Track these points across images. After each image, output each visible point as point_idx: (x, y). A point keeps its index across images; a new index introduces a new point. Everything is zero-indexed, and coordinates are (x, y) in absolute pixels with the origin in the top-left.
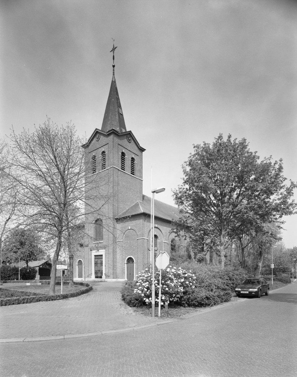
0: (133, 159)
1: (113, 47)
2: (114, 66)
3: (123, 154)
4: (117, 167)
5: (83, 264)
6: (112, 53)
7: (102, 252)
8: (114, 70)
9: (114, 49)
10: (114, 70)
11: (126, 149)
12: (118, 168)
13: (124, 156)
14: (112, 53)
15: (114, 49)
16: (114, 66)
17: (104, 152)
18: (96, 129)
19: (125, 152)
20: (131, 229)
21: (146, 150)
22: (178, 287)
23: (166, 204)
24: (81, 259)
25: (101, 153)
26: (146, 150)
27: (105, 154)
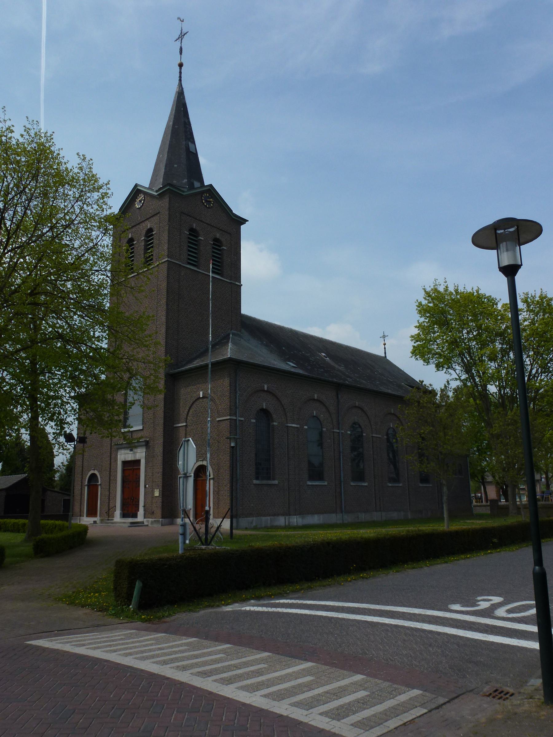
0: (217, 242)
1: (181, 33)
2: (181, 65)
3: (193, 232)
4: (177, 260)
5: (100, 483)
6: (178, 42)
7: (140, 454)
8: (180, 73)
9: (182, 36)
10: (180, 73)
11: (201, 221)
12: (180, 263)
13: (196, 237)
14: (178, 42)
15: (182, 36)
16: (181, 65)
17: (150, 230)
18: (136, 185)
19: (198, 229)
20: (267, 391)
21: (244, 221)
22: (482, 361)
23: (356, 349)
24: (96, 472)
25: (144, 232)
26: (244, 221)
27: (152, 235)
